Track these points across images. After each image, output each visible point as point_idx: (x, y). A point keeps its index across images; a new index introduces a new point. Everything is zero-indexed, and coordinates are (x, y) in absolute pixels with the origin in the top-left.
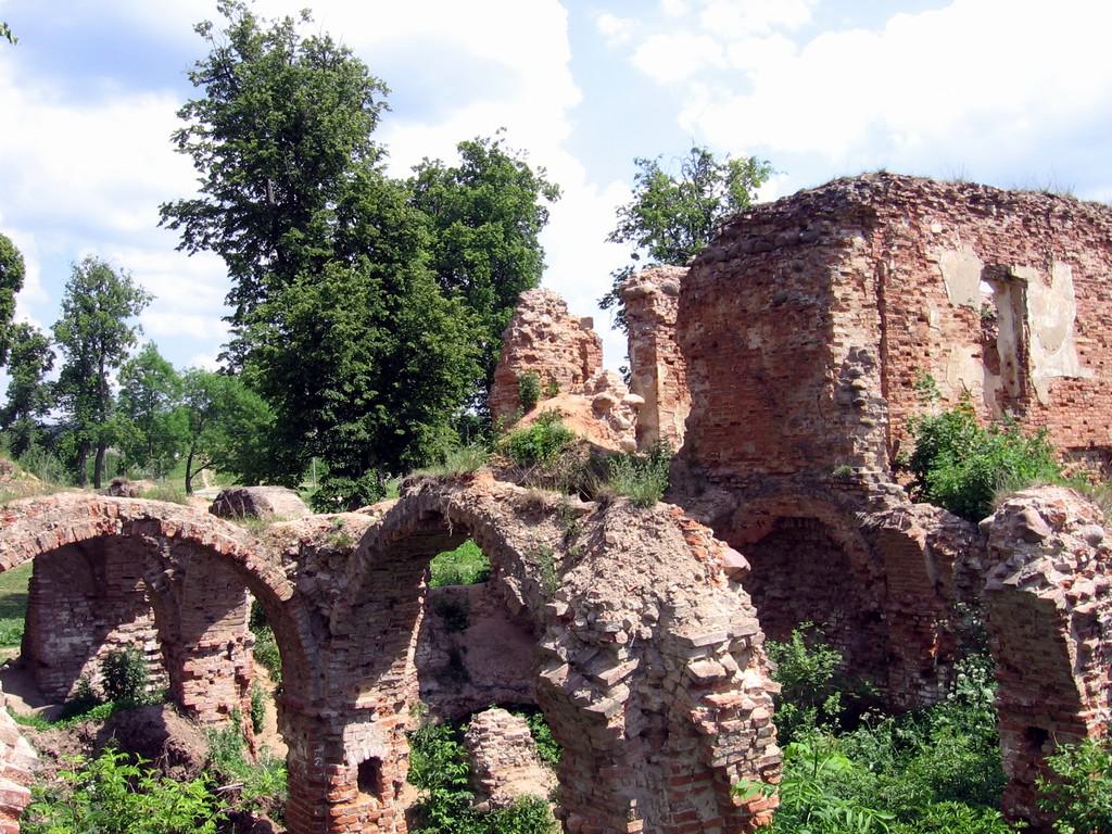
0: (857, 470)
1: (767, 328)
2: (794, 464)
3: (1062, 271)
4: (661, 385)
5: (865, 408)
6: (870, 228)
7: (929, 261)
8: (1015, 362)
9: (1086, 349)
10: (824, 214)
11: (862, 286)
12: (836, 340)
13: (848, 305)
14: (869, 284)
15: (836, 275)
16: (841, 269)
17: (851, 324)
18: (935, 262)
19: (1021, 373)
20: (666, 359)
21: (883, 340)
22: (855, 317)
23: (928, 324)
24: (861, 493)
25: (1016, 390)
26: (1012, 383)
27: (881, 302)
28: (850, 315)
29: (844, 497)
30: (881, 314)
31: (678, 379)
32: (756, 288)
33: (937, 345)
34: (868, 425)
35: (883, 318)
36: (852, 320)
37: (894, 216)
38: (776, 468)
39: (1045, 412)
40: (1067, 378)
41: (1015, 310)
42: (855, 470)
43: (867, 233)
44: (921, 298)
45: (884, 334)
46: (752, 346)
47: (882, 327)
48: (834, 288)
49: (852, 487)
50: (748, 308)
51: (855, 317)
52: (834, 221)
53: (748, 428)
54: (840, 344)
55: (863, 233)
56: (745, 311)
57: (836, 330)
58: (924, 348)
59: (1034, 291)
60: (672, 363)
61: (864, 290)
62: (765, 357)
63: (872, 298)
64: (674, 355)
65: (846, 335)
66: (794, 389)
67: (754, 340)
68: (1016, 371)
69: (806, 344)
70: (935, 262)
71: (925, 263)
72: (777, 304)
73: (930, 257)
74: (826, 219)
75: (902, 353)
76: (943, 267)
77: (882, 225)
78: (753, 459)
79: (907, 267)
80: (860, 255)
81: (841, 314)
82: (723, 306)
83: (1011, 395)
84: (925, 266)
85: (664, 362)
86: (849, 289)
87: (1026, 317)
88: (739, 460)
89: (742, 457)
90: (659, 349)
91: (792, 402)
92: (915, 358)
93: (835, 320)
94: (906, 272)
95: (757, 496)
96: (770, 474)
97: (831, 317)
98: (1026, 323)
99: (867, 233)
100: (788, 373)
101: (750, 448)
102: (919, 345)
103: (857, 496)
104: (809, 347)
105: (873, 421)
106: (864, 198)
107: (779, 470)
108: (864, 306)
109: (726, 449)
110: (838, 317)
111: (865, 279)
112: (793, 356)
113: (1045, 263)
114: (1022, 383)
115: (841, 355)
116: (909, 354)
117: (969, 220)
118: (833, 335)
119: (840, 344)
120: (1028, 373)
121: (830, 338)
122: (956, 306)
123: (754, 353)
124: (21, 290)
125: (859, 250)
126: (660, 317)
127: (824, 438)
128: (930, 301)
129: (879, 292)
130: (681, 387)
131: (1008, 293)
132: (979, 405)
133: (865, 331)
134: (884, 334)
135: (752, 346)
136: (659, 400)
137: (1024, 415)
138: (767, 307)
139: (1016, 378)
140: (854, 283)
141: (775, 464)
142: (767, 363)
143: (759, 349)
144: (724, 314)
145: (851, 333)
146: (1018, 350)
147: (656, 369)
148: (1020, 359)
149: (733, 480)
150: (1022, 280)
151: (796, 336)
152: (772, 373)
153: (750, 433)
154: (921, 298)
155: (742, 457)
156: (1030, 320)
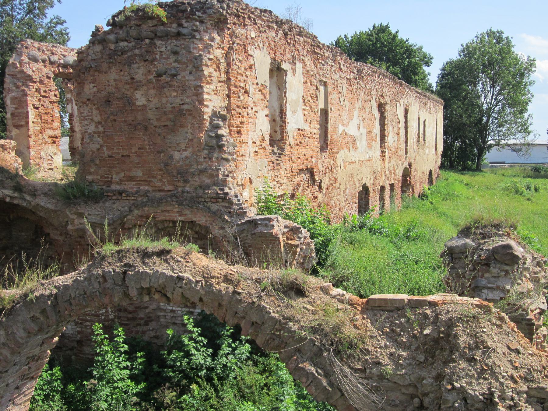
0: (223, 190)
1: (152, 92)
2: (174, 185)
3: (299, 66)
4: (31, 124)
5: (225, 149)
6: (223, 30)
7: (249, 55)
8: (278, 119)
9: (306, 113)
10: (197, 17)
11: (219, 68)
12: (205, 103)
13: (211, 80)
14: (222, 67)
15: (205, 60)
16: (208, 56)
17: (212, 93)
18: (252, 56)
19: (282, 126)
20: (33, 105)
21: (230, 103)
22: (215, 88)
23: (249, 96)
24: (227, 205)
25: (278, 136)
26: (276, 132)
27: (229, 79)
28: (212, 87)
29: (214, 207)
30: (228, 87)
31: (41, 119)
32: (142, 63)
33: (252, 108)
34: (227, 160)
35: (229, 90)
36: (213, 90)
37: (234, 24)
38: (159, 187)
39: (292, 150)
40: (299, 130)
41: (279, 89)
42: (220, 189)
43: (220, 33)
44: (246, 78)
45: (229, 100)
46: (139, 103)
47: (228, 96)
48: (204, 68)
49: (220, 200)
50: (136, 77)
51: (215, 88)
52: (202, 22)
53: (136, 159)
54: (207, 106)
55: (218, 33)
56: (133, 79)
57: (205, 96)
58: (247, 110)
59: (289, 78)
60: (37, 108)
61: (220, 70)
62: (149, 112)
63: (223, 77)
64: (39, 103)
65: (210, 100)
66: (172, 134)
67: (140, 99)
68: (278, 125)
69: (183, 104)
70: (252, 56)
71: (248, 56)
72: (159, 75)
73: (251, 53)
74: (197, 21)
75: (237, 113)
76: (255, 60)
77: (229, 29)
78: (140, 181)
79: (240, 58)
80: (219, 48)
81: (207, 86)
82: (114, 74)
83: (274, 139)
84: (247, 58)
85: (32, 107)
86: (212, 70)
87: (285, 93)
88: (128, 181)
89: (131, 179)
90: (29, 98)
91: (170, 143)
92: (243, 117)
93: (205, 90)
94: (240, 61)
95: (145, 206)
96: (153, 191)
97: (202, 87)
98: (285, 96)
99: (220, 33)
100: (168, 123)
101: (139, 173)
102: (244, 108)
103: (223, 206)
104: (185, 107)
105: (230, 157)
106: (223, 9)
107: (161, 188)
108: (220, 82)
109: (117, 174)
110: (207, 88)
111: (220, 63)
112: (171, 112)
113: (293, 61)
114: (282, 132)
115: (207, 112)
116: (240, 114)
117: (265, 31)
118: (203, 100)
119: (207, 106)
120: (285, 126)
121: (201, 102)
122: (260, 84)
123: (139, 108)
124: (91, 34)
125: (218, 44)
126: (29, 76)
127: (196, 167)
128: (249, 80)
129: (227, 73)
130: (43, 125)
131: (275, 78)
132: (267, 146)
133: (220, 98)
134: (229, 100)
135: (139, 103)
136: (30, 133)
137: (284, 151)
138: (152, 77)
139: (278, 129)
140: (214, 66)
141: (159, 184)
142: (151, 115)
143: (144, 106)
144: (115, 80)
145: (213, 102)
146: (280, 113)
147: (28, 112)
148: (281, 118)
149: (123, 195)
150: (285, 71)
151: (173, 98)
152: (156, 123)
153: (139, 163)
154: (246, 78)
155: (131, 179)
156: (287, 95)
